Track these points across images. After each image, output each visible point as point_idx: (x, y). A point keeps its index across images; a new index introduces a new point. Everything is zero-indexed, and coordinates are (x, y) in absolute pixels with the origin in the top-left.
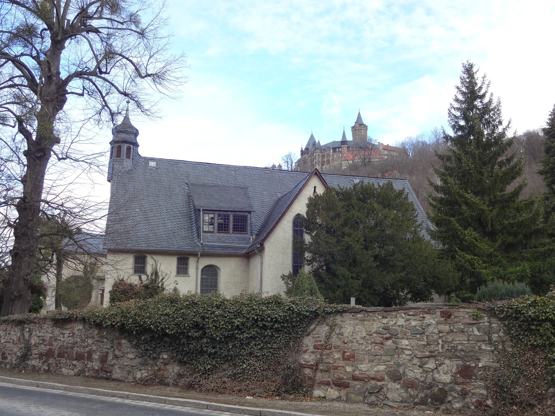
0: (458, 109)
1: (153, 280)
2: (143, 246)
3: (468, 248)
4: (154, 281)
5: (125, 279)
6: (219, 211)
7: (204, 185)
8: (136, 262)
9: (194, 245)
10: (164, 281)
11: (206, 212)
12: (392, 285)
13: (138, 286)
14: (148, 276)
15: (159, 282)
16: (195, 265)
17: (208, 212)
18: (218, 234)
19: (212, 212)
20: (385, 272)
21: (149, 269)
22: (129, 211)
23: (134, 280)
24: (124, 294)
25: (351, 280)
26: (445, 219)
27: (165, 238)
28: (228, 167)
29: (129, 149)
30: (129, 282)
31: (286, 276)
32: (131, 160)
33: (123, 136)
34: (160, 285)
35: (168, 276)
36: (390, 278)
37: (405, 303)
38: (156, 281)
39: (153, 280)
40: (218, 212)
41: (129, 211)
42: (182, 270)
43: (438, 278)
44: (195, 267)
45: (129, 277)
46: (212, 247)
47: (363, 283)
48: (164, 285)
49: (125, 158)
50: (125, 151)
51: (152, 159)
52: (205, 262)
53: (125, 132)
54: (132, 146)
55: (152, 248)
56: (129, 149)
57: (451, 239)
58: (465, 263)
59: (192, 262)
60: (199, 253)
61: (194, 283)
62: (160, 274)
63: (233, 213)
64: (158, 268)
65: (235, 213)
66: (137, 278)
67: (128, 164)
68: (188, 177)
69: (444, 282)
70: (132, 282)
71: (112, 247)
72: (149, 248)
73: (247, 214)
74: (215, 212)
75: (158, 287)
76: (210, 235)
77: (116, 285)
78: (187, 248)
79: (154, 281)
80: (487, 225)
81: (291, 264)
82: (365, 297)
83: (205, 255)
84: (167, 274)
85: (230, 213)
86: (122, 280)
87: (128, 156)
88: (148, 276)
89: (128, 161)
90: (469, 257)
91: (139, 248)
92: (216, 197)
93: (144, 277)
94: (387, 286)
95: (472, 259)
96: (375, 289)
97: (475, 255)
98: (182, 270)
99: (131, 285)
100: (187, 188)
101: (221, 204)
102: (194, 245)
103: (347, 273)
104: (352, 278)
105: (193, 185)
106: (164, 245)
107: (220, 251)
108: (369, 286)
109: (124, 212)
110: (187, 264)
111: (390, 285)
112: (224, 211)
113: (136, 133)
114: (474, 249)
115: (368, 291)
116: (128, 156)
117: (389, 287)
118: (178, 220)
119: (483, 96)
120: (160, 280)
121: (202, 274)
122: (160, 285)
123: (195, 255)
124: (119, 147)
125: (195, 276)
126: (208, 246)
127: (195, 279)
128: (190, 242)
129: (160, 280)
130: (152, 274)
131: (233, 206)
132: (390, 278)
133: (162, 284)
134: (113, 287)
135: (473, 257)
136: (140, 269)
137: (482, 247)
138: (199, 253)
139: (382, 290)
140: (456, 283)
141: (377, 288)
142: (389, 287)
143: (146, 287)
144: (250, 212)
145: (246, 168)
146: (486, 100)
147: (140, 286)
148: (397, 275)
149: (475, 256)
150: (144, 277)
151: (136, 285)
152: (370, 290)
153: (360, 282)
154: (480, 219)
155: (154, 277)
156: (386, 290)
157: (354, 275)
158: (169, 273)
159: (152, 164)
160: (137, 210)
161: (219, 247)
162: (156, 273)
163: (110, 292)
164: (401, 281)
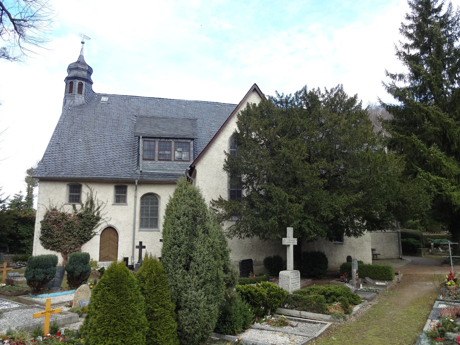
0: (411, 27)
1: (87, 209)
2: (78, 175)
3: (436, 168)
4: (89, 210)
5: (58, 208)
6: (160, 138)
7: (153, 117)
8: (71, 192)
9: (133, 172)
10: (99, 210)
11: (146, 139)
12: (345, 210)
13: (72, 216)
14: (82, 205)
15: (95, 212)
16: (134, 193)
17: (148, 139)
18: (159, 162)
19: (153, 140)
20: (335, 194)
21: (84, 198)
22: (72, 141)
23: (68, 209)
24: (56, 224)
25: (288, 204)
26: (401, 138)
27: (104, 166)
28: (179, 102)
29: (81, 85)
30: (62, 211)
31: (216, 202)
32: (83, 95)
33: (74, 73)
34: (96, 214)
35: (104, 205)
36: (341, 201)
37: (361, 232)
38: (91, 210)
39: (87, 209)
40: (159, 140)
41: (72, 141)
42: (120, 198)
43: (404, 202)
44: (134, 196)
45: (62, 207)
46: (152, 175)
47: (306, 207)
48: (100, 214)
49: (76, 93)
50: (77, 87)
51: (105, 95)
52: (144, 190)
53: (77, 69)
54: (84, 83)
55: (86, 176)
56: (81, 85)
57: (408, 160)
58: (430, 185)
59: (130, 192)
60: (137, 181)
61: (133, 211)
62: (95, 202)
63: (175, 140)
64: (94, 197)
65: (177, 140)
66: (71, 207)
67: (80, 99)
68: (138, 110)
69: (411, 206)
70: (66, 211)
71: (44, 176)
72: (83, 176)
73: (189, 141)
74: (156, 140)
75: (93, 216)
76: (150, 162)
77: (48, 215)
78: (123, 174)
79: (89, 210)
80: (453, 143)
81: (227, 189)
82: (308, 225)
83: (143, 183)
84: (103, 203)
85: (171, 140)
86: (55, 210)
87: (80, 91)
88: (82, 205)
89: (80, 96)
90: (434, 178)
91: (72, 176)
92: (161, 126)
93: (78, 206)
94: (339, 211)
95: (438, 180)
96: (321, 216)
97: (442, 175)
98: (120, 198)
99: (63, 214)
100: (135, 120)
101: (164, 132)
102: (133, 172)
103: (284, 194)
104: (291, 201)
105: (142, 117)
106: (100, 173)
107: (160, 179)
108: (314, 212)
109: (66, 142)
110: (125, 192)
111: (343, 210)
112: (165, 138)
113: (90, 71)
114: (441, 169)
115: (313, 218)
116: (80, 91)
117: (342, 213)
118: (121, 149)
119: (439, 9)
120: (95, 209)
121: (142, 203)
122: (96, 214)
123: (132, 182)
124: (71, 84)
125: (133, 205)
126: (147, 174)
127: (133, 207)
128: (128, 170)
129: (95, 209)
130: (87, 203)
131: (176, 134)
132: (341, 201)
133: (98, 214)
134: (45, 216)
135: (439, 178)
136: (74, 198)
137: (449, 166)
138: (137, 181)
139: (332, 216)
140: (427, 206)
141: (325, 214)
142: (342, 213)
143: (80, 216)
144: (192, 139)
145: (196, 102)
146: (441, 14)
147: (74, 216)
148: (351, 197)
149: (442, 177)
150: (78, 206)
151: (70, 215)
152: (315, 216)
153: (301, 206)
154: (445, 135)
155: (89, 206)
156: (337, 217)
157: (294, 197)
158: (105, 202)
159: (104, 99)
160: (80, 140)
161: (159, 174)
162: (91, 202)
163: (41, 222)
164: (356, 205)
